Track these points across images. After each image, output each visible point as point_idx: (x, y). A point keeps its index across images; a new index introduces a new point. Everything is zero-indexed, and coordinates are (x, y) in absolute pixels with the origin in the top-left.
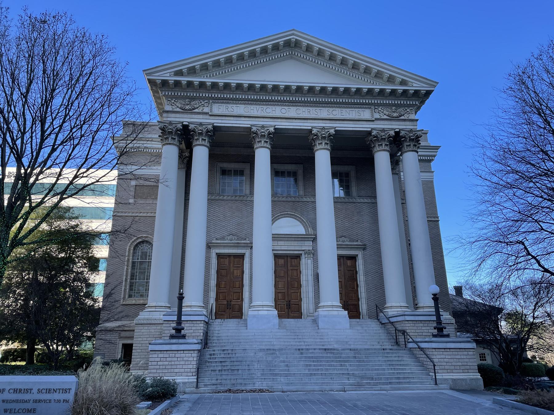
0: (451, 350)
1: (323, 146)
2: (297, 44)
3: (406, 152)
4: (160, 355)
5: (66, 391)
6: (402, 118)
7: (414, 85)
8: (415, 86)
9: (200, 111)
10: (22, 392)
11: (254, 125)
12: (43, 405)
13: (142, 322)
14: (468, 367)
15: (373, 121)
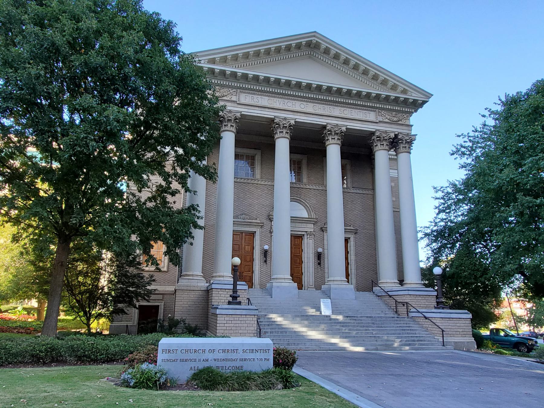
1: (284, 134)
2: (317, 46)
3: (402, 152)
4: (228, 319)
5: (266, 351)
6: (400, 122)
7: (413, 95)
8: (413, 96)
12: (248, 362)
14: (466, 333)
15: (377, 123)
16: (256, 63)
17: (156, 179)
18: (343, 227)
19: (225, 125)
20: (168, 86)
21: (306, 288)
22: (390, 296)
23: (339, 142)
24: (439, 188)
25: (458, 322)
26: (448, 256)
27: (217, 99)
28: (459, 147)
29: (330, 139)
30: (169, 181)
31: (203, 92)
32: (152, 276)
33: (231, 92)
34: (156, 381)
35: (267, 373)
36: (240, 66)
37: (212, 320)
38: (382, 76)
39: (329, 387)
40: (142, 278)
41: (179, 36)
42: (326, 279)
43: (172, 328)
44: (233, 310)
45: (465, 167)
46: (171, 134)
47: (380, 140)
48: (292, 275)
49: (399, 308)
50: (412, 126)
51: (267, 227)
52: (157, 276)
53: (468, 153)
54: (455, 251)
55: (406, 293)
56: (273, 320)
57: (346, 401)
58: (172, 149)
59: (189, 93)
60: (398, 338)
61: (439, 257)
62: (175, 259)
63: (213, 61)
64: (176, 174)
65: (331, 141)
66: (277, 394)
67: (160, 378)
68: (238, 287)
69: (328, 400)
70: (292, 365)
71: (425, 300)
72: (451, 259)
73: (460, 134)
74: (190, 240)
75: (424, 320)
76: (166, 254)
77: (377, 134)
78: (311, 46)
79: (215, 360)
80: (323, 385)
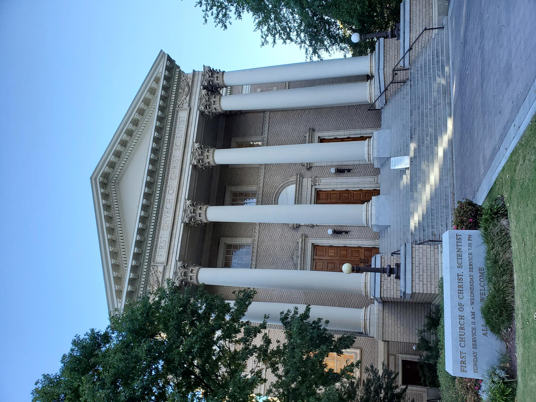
0: (412, 18)
2: (106, 176)
3: (223, 81)
4: (417, 280)
5: (459, 239)
7: (161, 71)
8: (162, 71)
9: (161, 275)
11: (183, 219)
12: (474, 261)
13: (381, 333)
15: (190, 109)
16: (123, 244)
17: (252, 364)
18: (307, 144)
19: (191, 279)
20: (141, 350)
21: (378, 185)
22: (386, 89)
23: (211, 150)
24: (263, 39)
25: (414, 14)
26: (339, 28)
27: (160, 289)
28: (218, 20)
29: (208, 160)
30: (253, 349)
31: (150, 307)
32: (367, 370)
33: (153, 272)
34: (505, 383)
35: (487, 238)
36: (125, 262)
37: (419, 298)
38: (140, 105)
39: (502, 160)
40: (369, 380)
41: (90, 332)
42: (367, 162)
43: (432, 348)
44: (407, 273)
45: (240, 13)
46: (197, 346)
47: (209, 105)
48: (362, 202)
49: (399, 80)
50: (194, 71)
51: (307, 231)
52: (366, 364)
53: (224, 11)
54: (333, 20)
55: (381, 72)
56: (417, 225)
57: (522, 140)
58: (215, 343)
59: (152, 323)
60: (435, 79)
61: (339, 37)
62: (347, 341)
63: (119, 293)
64: (244, 340)
65: (210, 159)
66: (516, 227)
67: (500, 377)
68: (378, 266)
69: (521, 162)
70: (475, 205)
71: (389, 52)
72: (341, 24)
73: (204, 19)
74: (322, 323)
75: (414, 51)
76: (340, 353)
77: (203, 108)
78: (106, 182)
79: (472, 303)
80: (500, 168)
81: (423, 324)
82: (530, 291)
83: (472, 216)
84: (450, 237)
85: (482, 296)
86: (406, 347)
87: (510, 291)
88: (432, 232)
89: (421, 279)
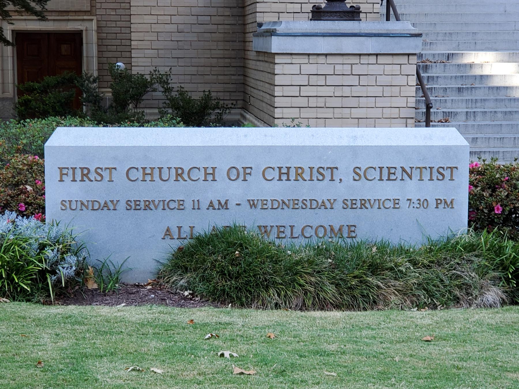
4: (308, 69)
5: (442, 173)
10: (306, 176)
12: (372, 213)
34: (43, 273)
35: (443, 252)
43: (124, 102)
56: (477, 72)
67: (57, 263)
79: (253, 204)
81: (187, 87)
82: (298, 347)
83: (511, 213)
84: (446, 150)
85: (275, 230)
86: (118, 42)
87: (295, 301)
88: (456, 114)
89: (314, 80)
